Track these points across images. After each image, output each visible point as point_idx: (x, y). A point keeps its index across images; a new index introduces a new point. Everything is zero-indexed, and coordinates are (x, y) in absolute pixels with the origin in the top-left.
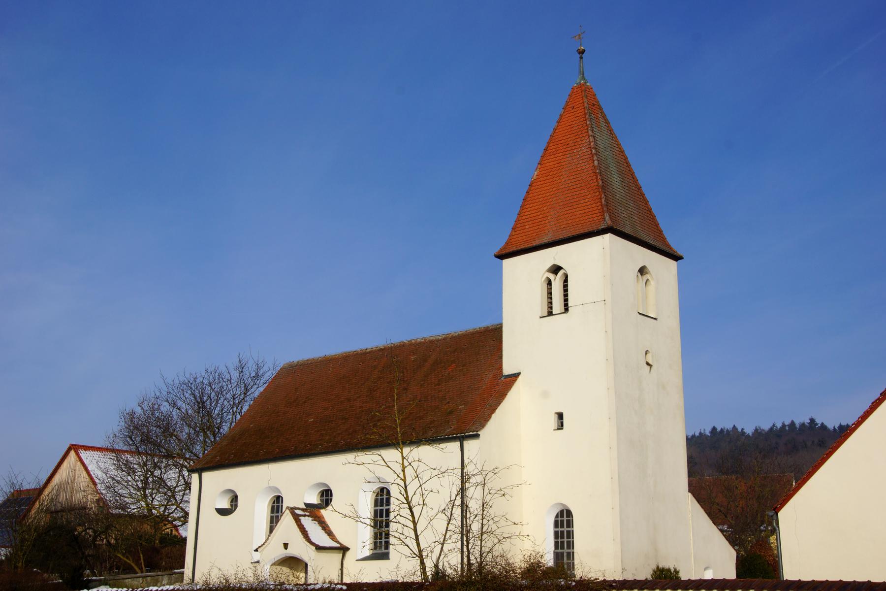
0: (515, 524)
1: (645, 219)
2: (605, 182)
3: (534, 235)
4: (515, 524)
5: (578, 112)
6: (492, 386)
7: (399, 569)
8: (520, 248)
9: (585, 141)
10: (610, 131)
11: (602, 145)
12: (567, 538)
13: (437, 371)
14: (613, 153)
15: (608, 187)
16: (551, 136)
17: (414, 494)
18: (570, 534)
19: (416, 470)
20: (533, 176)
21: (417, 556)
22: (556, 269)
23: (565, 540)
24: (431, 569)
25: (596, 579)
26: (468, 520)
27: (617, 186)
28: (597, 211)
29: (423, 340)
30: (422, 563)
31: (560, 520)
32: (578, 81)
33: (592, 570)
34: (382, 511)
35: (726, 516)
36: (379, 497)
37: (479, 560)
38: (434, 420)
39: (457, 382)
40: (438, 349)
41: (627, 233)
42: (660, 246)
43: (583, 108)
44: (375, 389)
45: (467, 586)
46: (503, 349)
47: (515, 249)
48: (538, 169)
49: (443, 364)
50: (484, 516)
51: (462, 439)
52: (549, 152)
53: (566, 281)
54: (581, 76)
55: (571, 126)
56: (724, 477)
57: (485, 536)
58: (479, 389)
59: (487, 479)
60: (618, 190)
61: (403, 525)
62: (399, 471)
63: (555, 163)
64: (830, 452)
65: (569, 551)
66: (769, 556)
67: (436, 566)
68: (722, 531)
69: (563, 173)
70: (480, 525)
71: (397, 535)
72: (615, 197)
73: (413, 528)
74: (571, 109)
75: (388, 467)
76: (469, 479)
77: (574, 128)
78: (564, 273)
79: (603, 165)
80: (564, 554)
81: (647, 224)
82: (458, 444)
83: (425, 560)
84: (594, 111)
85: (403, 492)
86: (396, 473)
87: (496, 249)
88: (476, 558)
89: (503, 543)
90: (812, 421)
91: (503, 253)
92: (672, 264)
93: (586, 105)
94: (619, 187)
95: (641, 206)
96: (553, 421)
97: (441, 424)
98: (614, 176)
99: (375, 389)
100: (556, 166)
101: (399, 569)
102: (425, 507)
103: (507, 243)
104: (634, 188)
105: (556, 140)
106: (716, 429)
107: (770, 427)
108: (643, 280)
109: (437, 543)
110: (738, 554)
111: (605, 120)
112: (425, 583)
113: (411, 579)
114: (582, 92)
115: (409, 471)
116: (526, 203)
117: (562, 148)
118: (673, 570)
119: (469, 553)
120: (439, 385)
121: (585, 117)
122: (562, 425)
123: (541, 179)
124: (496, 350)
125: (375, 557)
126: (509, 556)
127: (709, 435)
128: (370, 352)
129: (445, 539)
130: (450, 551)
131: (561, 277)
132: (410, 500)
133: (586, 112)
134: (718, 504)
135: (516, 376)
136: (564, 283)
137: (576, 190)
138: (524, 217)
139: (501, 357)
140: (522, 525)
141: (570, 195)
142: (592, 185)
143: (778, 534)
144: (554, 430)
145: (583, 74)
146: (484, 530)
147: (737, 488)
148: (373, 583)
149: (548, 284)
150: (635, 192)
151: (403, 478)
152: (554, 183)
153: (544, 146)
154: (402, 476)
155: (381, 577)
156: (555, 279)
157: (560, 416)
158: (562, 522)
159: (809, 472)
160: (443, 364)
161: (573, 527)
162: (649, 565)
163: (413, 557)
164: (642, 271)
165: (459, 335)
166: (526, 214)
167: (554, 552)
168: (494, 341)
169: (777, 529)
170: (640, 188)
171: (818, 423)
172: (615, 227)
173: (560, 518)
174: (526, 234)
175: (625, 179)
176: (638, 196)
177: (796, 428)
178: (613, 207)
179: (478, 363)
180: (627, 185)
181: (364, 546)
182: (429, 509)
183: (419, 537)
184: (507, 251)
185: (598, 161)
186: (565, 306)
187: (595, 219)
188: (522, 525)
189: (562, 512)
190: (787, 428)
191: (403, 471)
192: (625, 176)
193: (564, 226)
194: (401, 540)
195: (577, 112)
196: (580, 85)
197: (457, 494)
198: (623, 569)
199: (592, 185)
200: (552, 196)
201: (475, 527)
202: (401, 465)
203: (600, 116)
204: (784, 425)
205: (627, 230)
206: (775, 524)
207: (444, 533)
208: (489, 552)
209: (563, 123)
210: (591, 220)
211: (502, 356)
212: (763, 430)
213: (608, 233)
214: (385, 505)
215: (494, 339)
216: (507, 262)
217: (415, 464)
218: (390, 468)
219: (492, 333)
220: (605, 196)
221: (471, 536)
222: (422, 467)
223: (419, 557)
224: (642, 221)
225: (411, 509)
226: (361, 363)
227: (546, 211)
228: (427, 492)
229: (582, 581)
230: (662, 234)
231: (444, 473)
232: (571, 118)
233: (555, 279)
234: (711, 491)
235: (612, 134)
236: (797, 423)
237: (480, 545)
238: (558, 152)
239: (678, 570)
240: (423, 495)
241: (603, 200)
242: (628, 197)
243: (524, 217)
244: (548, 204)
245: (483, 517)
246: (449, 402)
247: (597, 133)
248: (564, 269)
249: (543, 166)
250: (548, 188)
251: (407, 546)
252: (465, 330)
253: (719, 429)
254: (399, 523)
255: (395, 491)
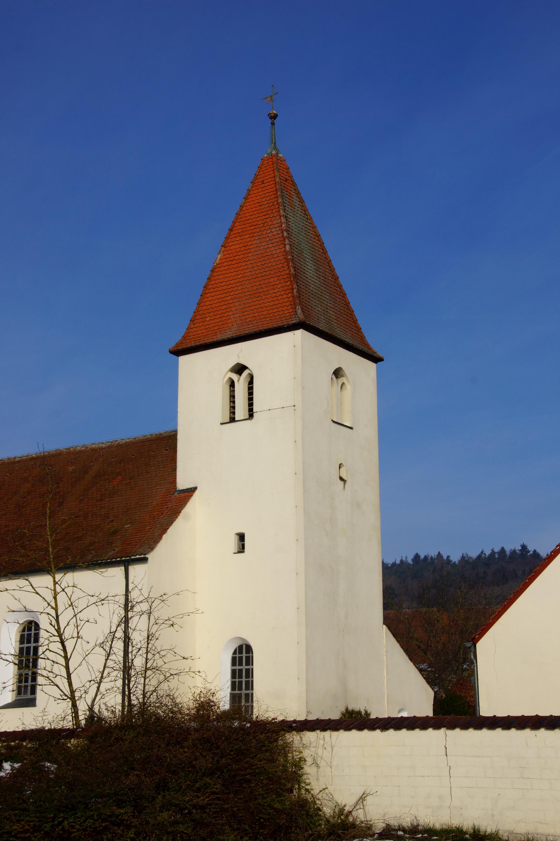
0: (184, 658)
1: (342, 315)
2: (298, 270)
3: (216, 328)
4: (184, 658)
5: (269, 187)
6: (164, 502)
7: (46, 714)
8: (199, 343)
9: (275, 222)
10: (305, 211)
11: (296, 227)
12: (246, 678)
13: (99, 485)
14: (308, 237)
15: (301, 276)
16: (236, 214)
17: (67, 625)
18: (249, 673)
19: (70, 597)
20: (216, 261)
21: (68, 697)
22: (240, 369)
23: (244, 679)
24: (85, 712)
25: (273, 719)
26: (130, 655)
27: (311, 275)
28: (288, 304)
29: (84, 448)
30: (74, 706)
31: (239, 657)
32: (269, 151)
33: (270, 709)
34: (28, 649)
35: (425, 653)
36: (26, 633)
37: (141, 700)
38: (94, 542)
39: (123, 497)
40: (101, 459)
41: (322, 330)
42: (358, 345)
43: (274, 182)
44: (24, 505)
45: (126, 731)
46: (178, 459)
47: (193, 344)
48: (221, 253)
49: (107, 477)
50: (149, 649)
51: (126, 563)
52: (235, 232)
53: (251, 382)
54: (273, 145)
55: (260, 204)
56: (424, 609)
57: (149, 673)
58: (148, 505)
59: (153, 608)
60: (313, 279)
61: (53, 661)
62: (50, 598)
63: (241, 245)
64: (532, 576)
65: (247, 692)
66: (470, 696)
67: (91, 709)
68: (421, 671)
69: (250, 258)
70: (144, 660)
71: (45, 673)
72: (309, 287)
73: (64, 665)
74: (260, 183)
75: (37, 593)
76: (132, 607)
77: (264, 206)
78: (249, 373)
79: (296, 250)
80: (241, 695)
81: (345, 319)
82: (123, 568)
83: (78, 702)
84: (286, 186)
85: (54, 622)
86: (46, 601)
87: (172, 344)
88: (137, 699)
89: (170, 680)
90: (524, 547)
91: (179, 348)
92: (371, 366)
93: (278, 180)
94: (313, 276)
95: (337, 299)
96: (233, 543)
97: (103, 545)
98: (309, 264)
99: (24, 505)
100: (242, 249)
101: (46, 714)
102: (79, 640)
103: (184, 337)
104: (330, 278)
105: (243, 220)
106: (419, 557)
107: (478, 555)
108: (337, 383)
109: (93, 682)
110: (435, 693)
111: (299, 198)
112: (76, 729)
113: (60, 725)
114: (273, 164)
115: (62, 597)
116: (207, 291)
117: (249, 228)
118: (363, 713)
119: (130, 693)
120: (101, 500)
121: (277, 194)
122: (243, 547)
123: (225, 264)
124: (169, 460)
125: (20, 703)
126: (175, 696)
127: (412, 563)
128: (19, 462)
129: (102, 677)
130: (108, 691)
131: (245, 378)
132: (62, 632)
133: (278, 187)
134: (417, 640)
135: (193, 490)
136: (249, 385)
137: (265, 278)
138: (204, 308)
139: (174, 469)
140: (193, 660)
141: (257, 284)
142: (283, 273)
143: (476, 667)
144: (234, 553)
145: (275, 144)
146: (148, 665)
147: (438, 621)
148: (14, 731)
149: (230, 386)
150: (332, 283)
151: (54, 607)
152: (240, 269)
153: (229, 225)
154: (53, 604)
155: (23, 724)
156: (238, 380)
157: (241, 537)
158: (241, 658)
159: (510, 599)
160: (107, 477)
161: (252, 665)
162: (337, 707)
163: (63, 699)
164: (338, 373)
165: (126, 442)
166: (207, 304)
167: (231, 694)
168: (167, 450)
169: (475, 662)
170: (336, 278)
171: (530, 549)
172: (308, 322)
173: (239, 654)
174: (207, 327)
175: (320, 267)
176: (335, 288)
177: (506, 555)
178: (306, 299)
179: (148, 476)
180: (322, 275)
181: (4, 688)
182: (84, 643)
183: (72, 676)
184: (184, 346)
185: (290, 245)
186: (249, 412)
187: (286, 312)
188: (193, 660)
189: (240, 647)
190: (497, 556)
191: (55, 598)
192: (321, 264)
193: (250, 319)
194: (50, 680)
195: (267, 188)
196: (271, 156)
197: (119, 624)
198: (307, 712)
199: (283, 273)
200: (237, 285)
201: (138, 662)
202: (53, 592)
203: (293, 194)
204: (493, 553)
205: (322, 326)
206: (472, 657)
207: (101, 670)
208: (154, 691)
209: (251, 199)
210: (281, 313)
211: (176, 468)
212: (471, 558)
213: (299, 329)
214: (33, 635)
215: (168, 448)
216: (184, 360)
217: (69, 591)
218: (39, 594)
219: (165, 441)
220: (297, 286)
221: (133, 673)
222: (77, 593)
223: (70, 699)
224: (338, 316)
225: (62, 643)
226: (8, 474)
227: (230, 302)
228: (83, 623)
229: (258, 721)
230: (361, 332)
231: (103, 600)
232: (260, 194)
233: (238, 380)
234: (410, 625)
235: (307, 216)
236: (508, 549)
237: (143, 683)
238: (245, 233)
239: (369, 712)
240: (77, 626)
241: (295, 291)
242: (323, 288)
243: (204, 308)
244: (232, 293)
245: (147, 650)
246: (112, 521)
247: (289, 213)
248: (250, 370)
249: (227, 249)
250: (233, 274)
251: (57, 686)
252: (134, 437)
253: (422, 557)
254: (48, 659)
255: (44, 622)
